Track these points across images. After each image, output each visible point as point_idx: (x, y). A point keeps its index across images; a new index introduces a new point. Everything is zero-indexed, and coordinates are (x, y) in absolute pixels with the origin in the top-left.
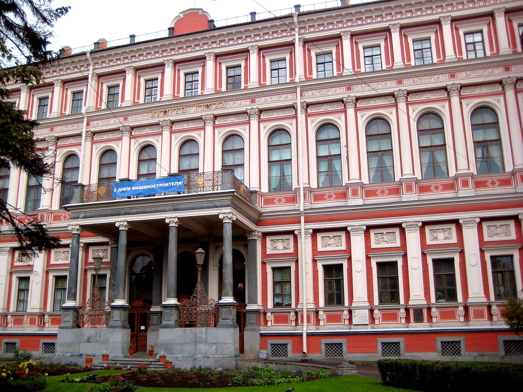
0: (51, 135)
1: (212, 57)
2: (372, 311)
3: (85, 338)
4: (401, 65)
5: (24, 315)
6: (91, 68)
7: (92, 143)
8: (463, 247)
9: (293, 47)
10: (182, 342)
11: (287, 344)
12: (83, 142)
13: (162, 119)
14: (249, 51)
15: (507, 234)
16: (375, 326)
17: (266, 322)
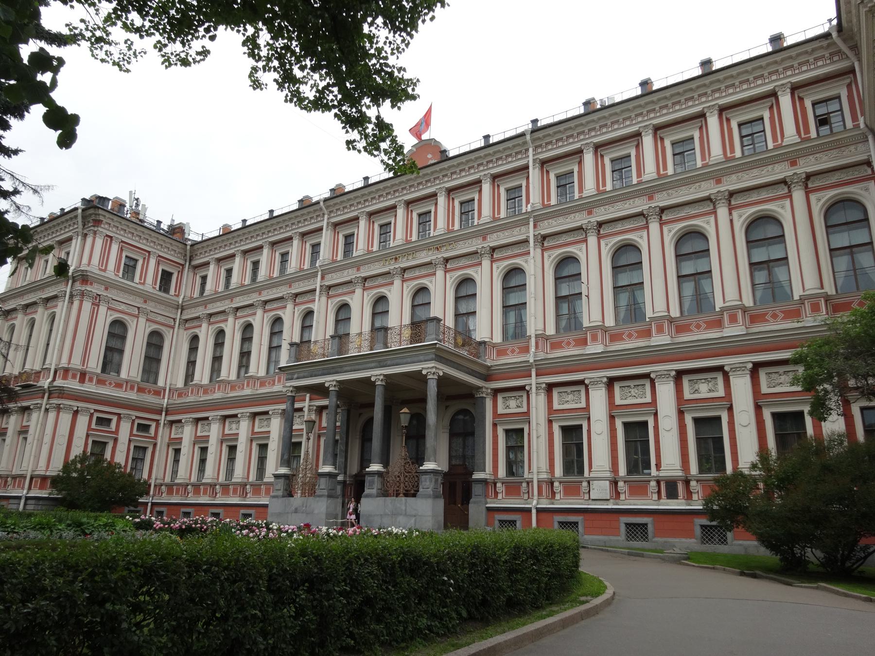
1: (650, 131)
2: (615, 483)
4: (655, 176)
6: (326, 217)
7: (543, 251)
8: (731, 401)
9: (703, 119)
12: (317, 298)
13: (392, 267)
15: (644, 395)
16: (555, 502)
17: (496, 494)
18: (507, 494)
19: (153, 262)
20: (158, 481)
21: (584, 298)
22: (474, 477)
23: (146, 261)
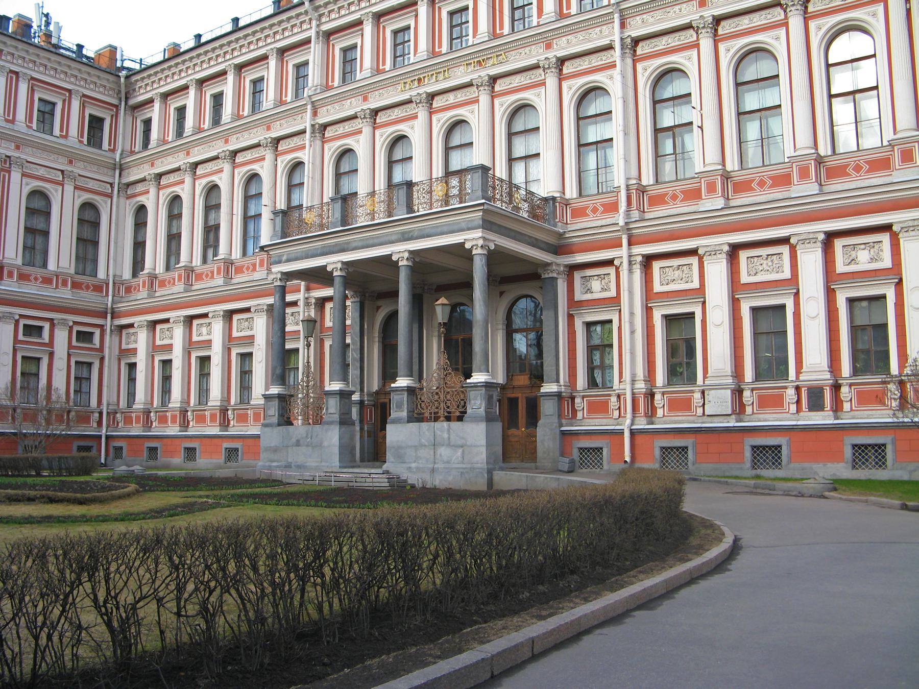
2: (738, 392)
3: (294, 440)
11: (601, 449)
15: (780, 269)
18: (589, 412)
19: (76, 104)
20: (111, 407)
22: (543, 390)
23: (67, 103)
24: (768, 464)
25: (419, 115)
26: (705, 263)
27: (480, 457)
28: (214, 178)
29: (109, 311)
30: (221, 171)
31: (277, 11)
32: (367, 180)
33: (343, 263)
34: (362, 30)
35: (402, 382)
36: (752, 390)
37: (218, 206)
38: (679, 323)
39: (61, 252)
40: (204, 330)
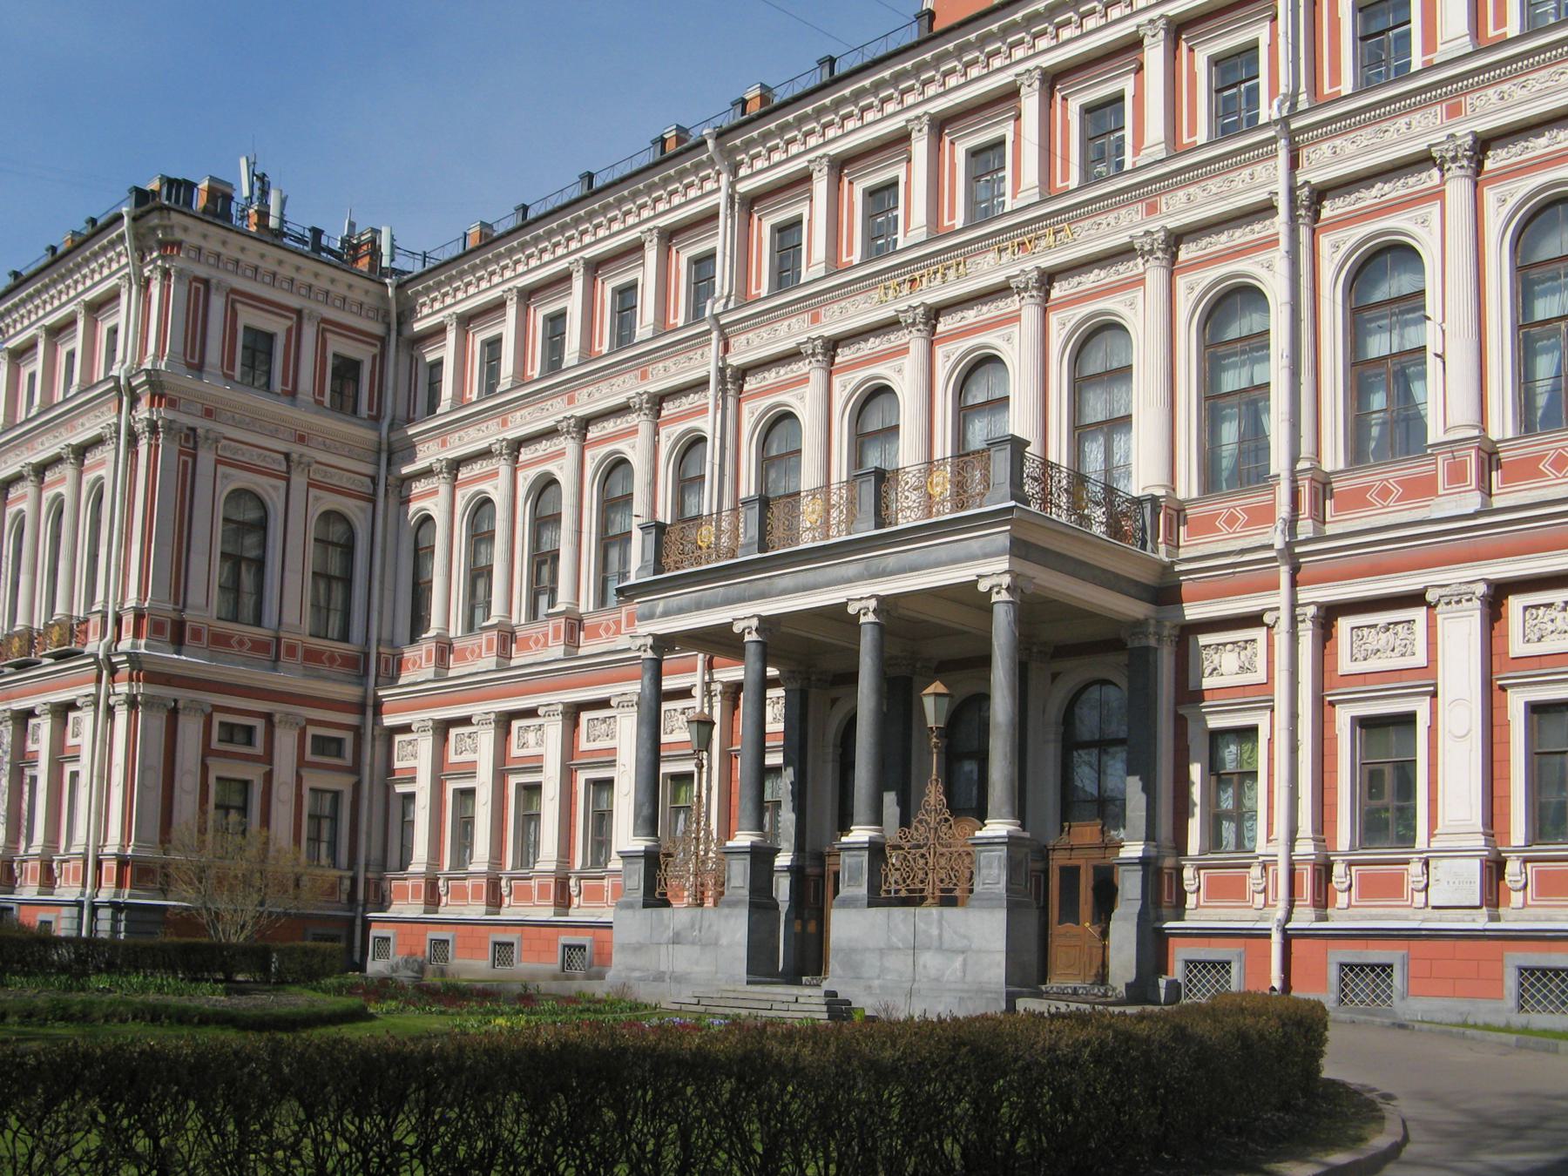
0: (814, 334)
2: (1494, 869)
5: (1248, 866)
10: (882, 945)
11: (1229, 963)
13: (903, 306)
14: (1141, 41)
21: (1432, 364)
24: (1551, 1002)
25: (811, 376)
26: (1439, 618)
27: (993, 969)
28: (550, 467)
29: (370, 702)
30: (495, 474)
31: (926, 34)
32: (821, 462)
33: (760, 618)
34: (810, 191)
35: (860, 834)
36: (1350, 864)
37: (556, 519)
38: (1387, 732)
39: (292, 598)
40: (531, 737)
